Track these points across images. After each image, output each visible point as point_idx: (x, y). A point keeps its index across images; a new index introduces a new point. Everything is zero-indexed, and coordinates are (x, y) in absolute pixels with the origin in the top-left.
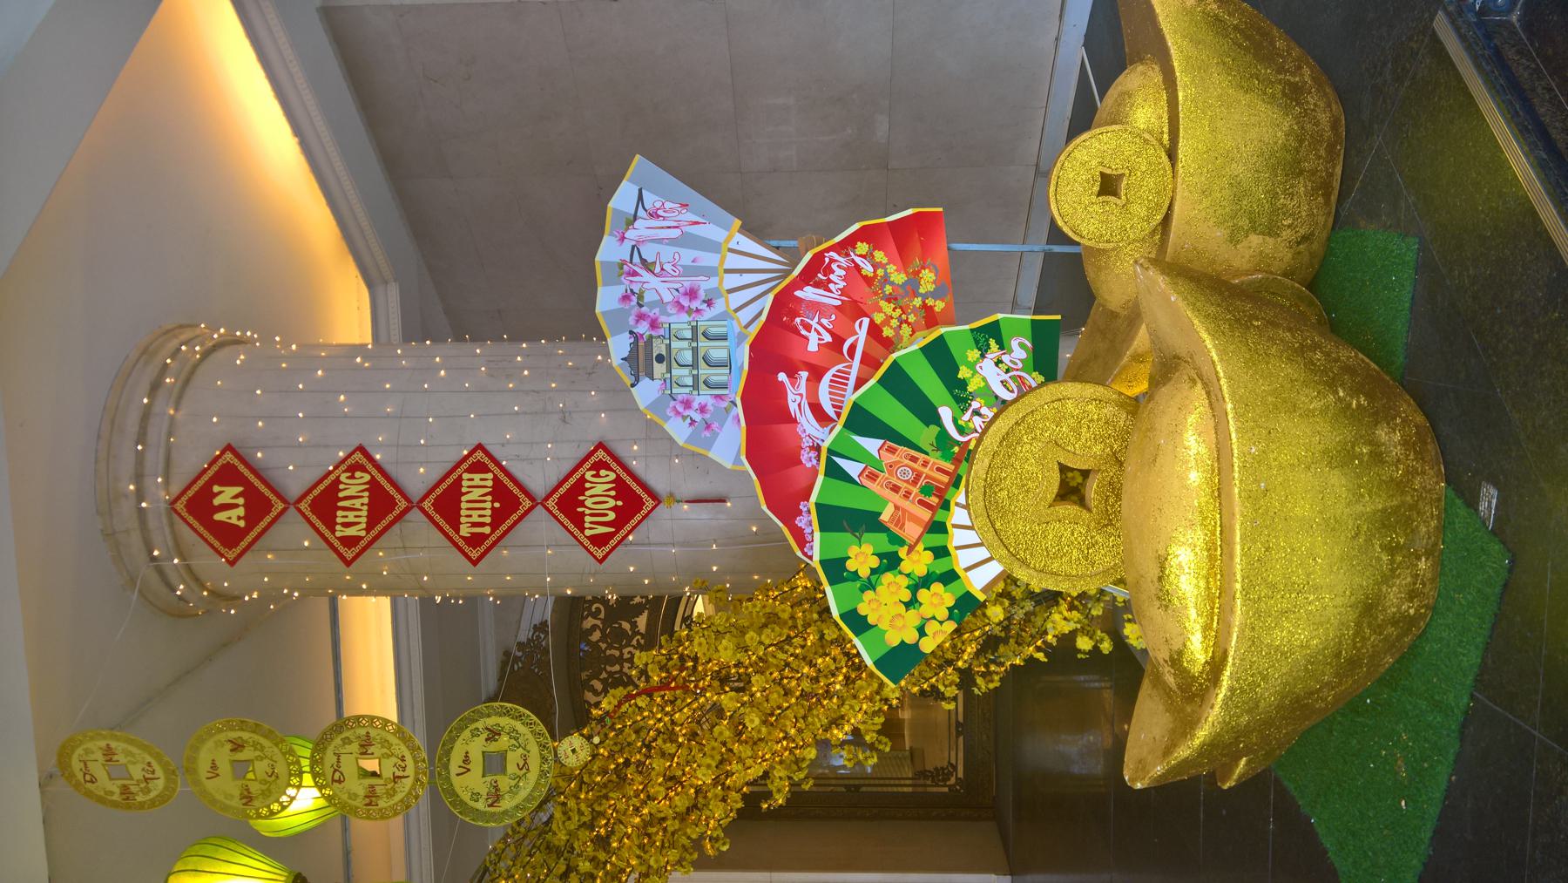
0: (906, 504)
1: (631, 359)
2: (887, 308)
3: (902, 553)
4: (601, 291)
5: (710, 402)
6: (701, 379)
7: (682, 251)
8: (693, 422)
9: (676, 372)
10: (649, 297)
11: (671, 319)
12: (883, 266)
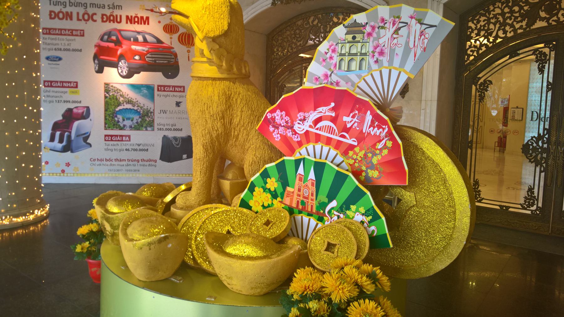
1: (355, 24)
2: (361, 154)
3: (279, 199)
4: (387, 8)
5: (333, 62)
6: (343, 57)
7: (402, 48)
8: (326, 53)
9: (348, 45)
10: (382, 31)
11: (371, 43)
12: (380, 153)
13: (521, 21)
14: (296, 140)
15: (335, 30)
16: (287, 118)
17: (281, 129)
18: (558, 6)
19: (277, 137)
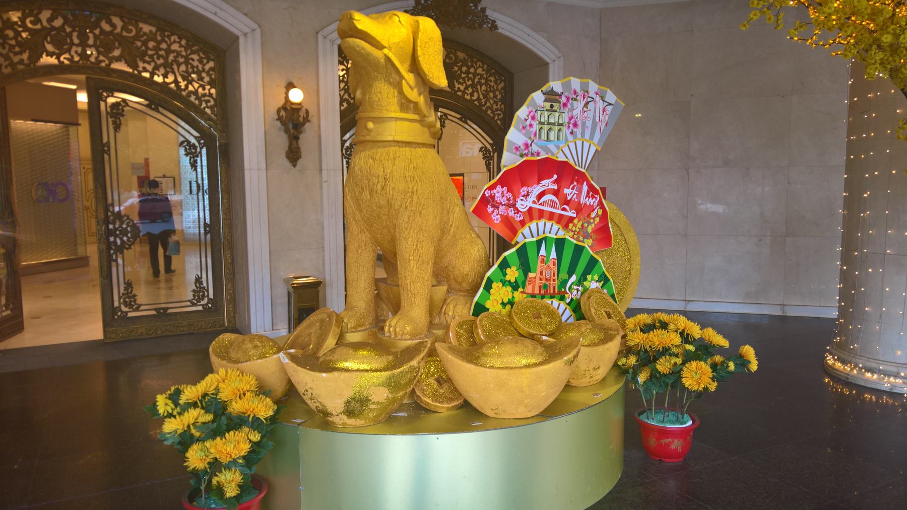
0: (538, 281)
2: (579, 226)
3: (520, 290)
5: (533, 130)
8: (526, 120)
13: (21, 53)
14: (518, 219)
15: (534, 95)
16: (509, 195)
17: (502, 208)
18: (68, 40)
19: (496, 218)
